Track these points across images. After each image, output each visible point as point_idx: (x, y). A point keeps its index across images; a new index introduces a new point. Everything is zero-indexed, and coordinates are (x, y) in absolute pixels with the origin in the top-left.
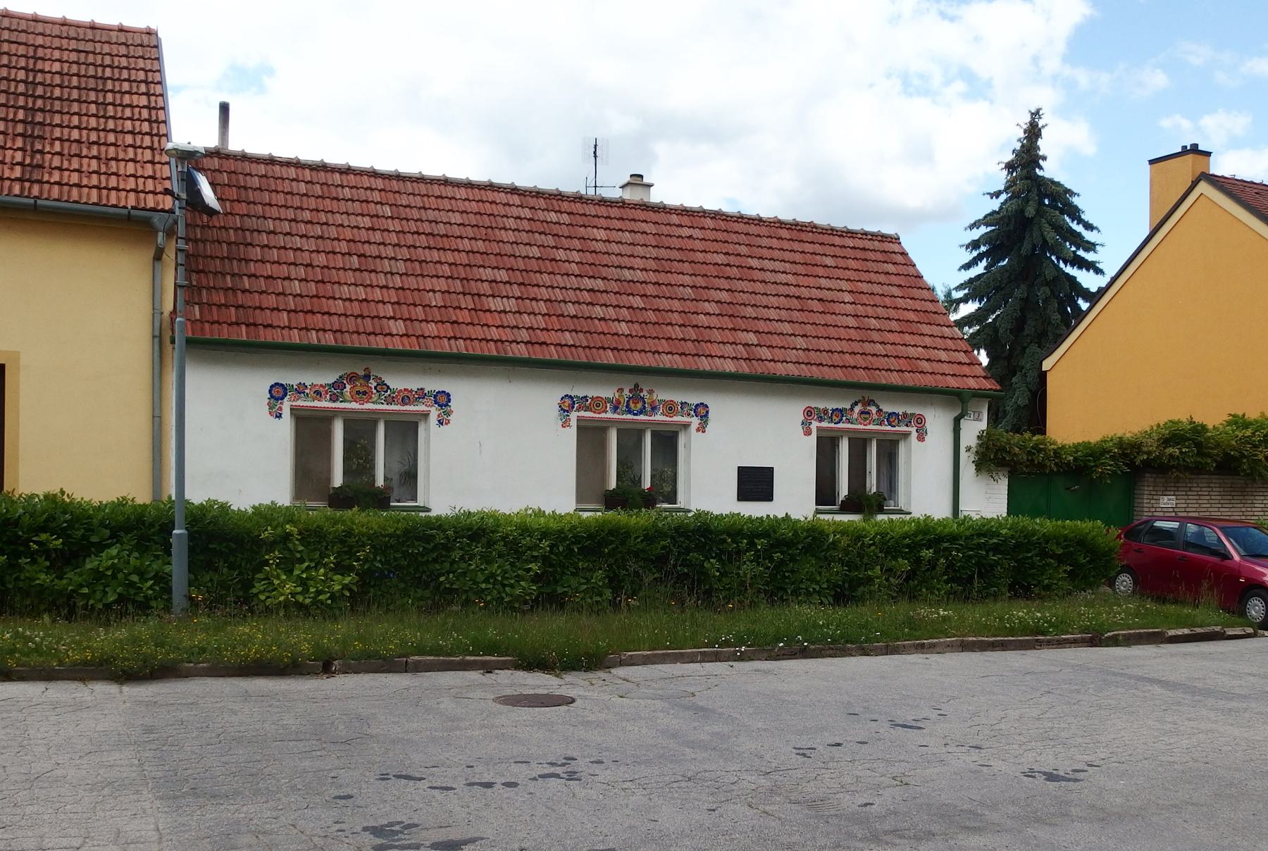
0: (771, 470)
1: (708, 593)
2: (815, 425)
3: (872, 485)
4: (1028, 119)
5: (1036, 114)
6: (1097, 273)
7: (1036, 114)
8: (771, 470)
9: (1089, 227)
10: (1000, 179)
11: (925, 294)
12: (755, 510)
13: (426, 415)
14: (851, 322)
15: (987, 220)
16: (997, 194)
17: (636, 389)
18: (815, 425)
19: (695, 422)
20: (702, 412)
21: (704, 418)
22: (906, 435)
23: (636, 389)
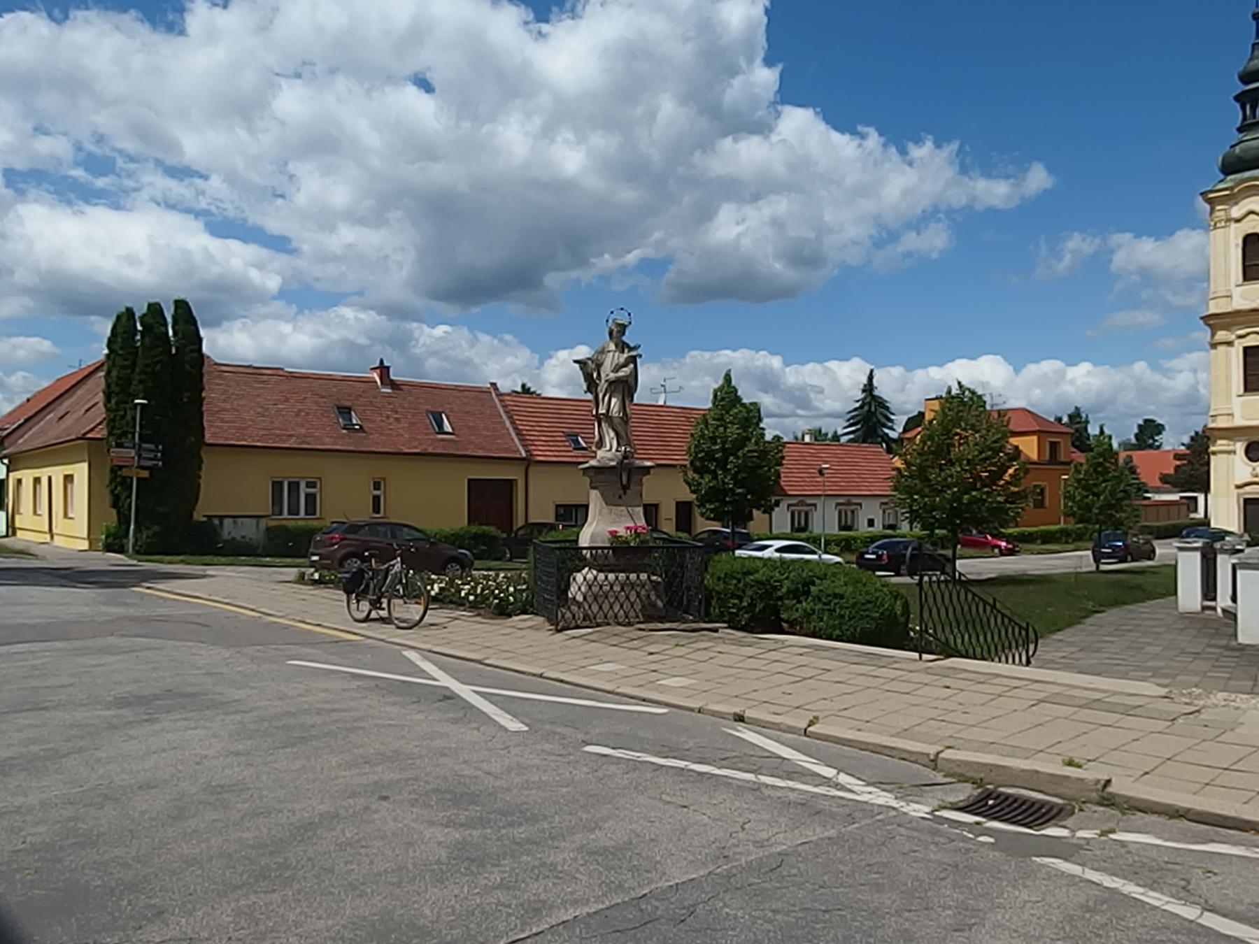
3: (849, 523)
10: (860, 396)
16: (858, 401)
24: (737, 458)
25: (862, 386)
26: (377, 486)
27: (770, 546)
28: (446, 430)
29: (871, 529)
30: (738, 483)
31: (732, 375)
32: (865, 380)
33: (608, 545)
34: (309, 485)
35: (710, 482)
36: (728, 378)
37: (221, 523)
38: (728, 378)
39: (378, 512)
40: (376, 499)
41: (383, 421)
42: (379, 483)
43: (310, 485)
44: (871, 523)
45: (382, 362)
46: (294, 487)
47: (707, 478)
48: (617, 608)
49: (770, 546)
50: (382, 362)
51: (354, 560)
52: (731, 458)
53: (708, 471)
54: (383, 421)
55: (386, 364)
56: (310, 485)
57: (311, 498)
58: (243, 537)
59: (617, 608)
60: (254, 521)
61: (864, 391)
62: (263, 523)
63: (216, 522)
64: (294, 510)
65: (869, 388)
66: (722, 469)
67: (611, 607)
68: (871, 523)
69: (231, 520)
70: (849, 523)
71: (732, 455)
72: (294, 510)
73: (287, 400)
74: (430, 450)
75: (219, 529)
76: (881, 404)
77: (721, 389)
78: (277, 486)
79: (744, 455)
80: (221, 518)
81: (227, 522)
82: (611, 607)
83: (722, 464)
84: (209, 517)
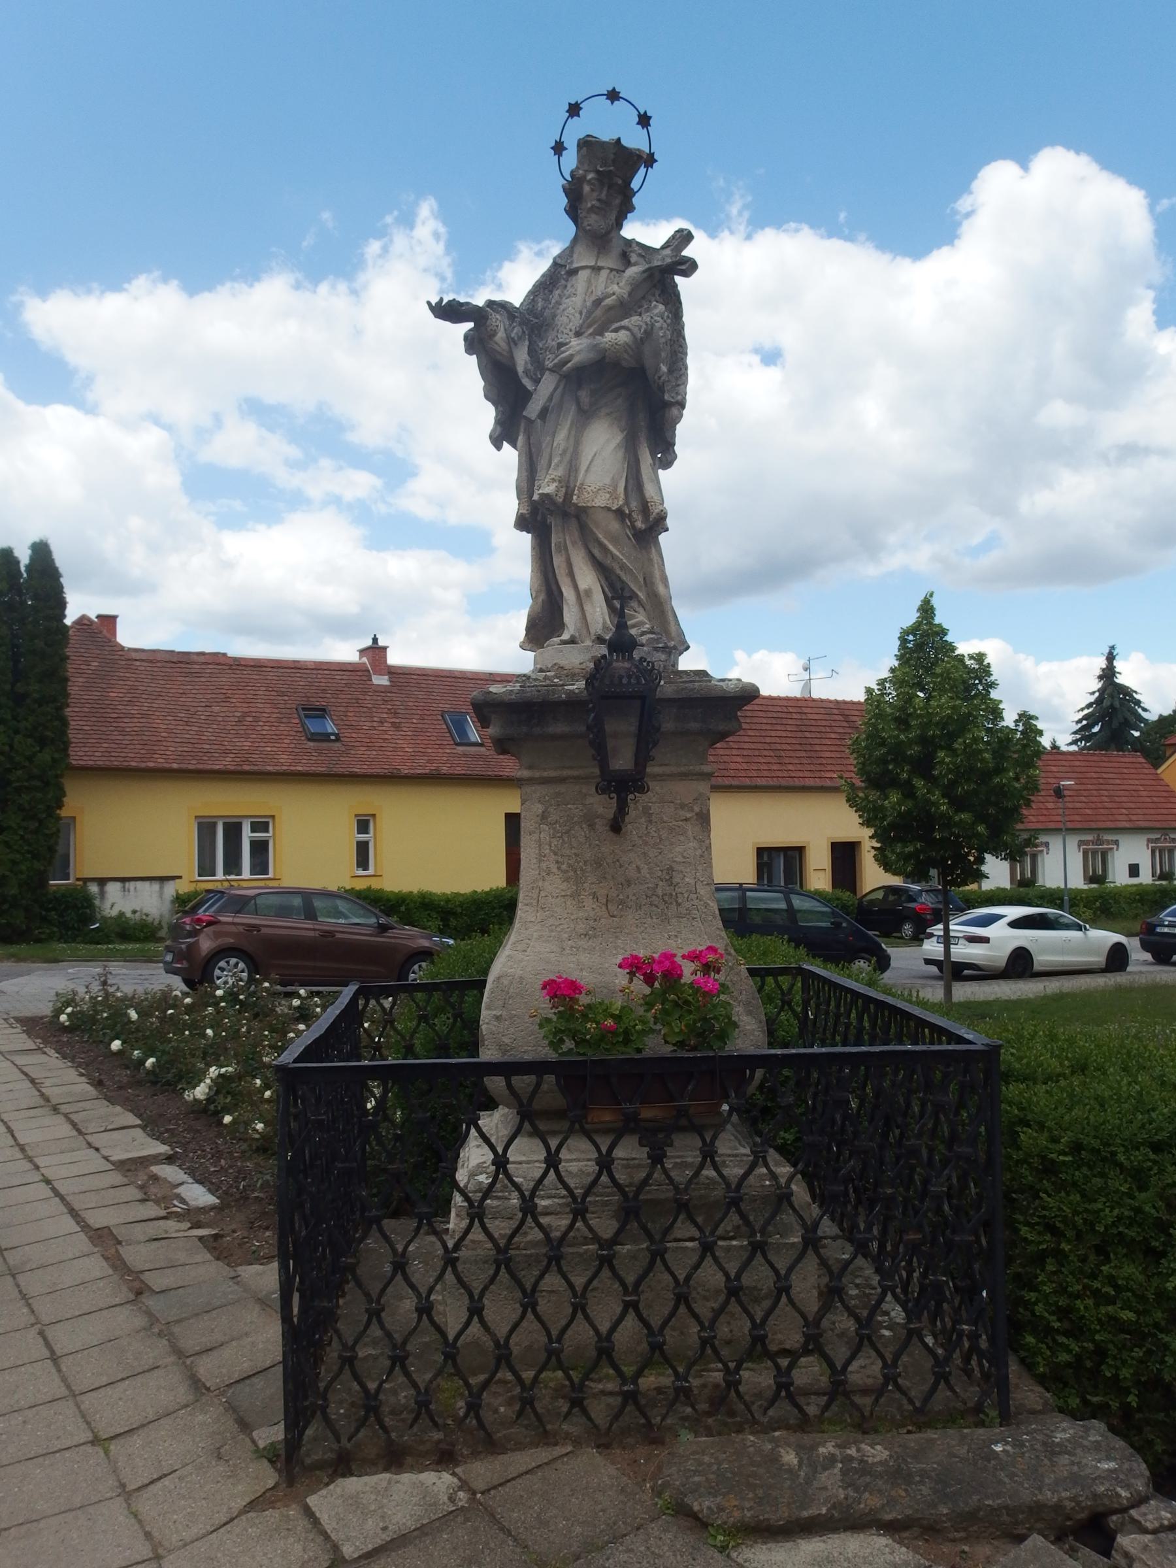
0: (1138, 865)
1: (251, 1228)
2: (1150, 845)
3: (1167, 868)
4: (1107, 650)
5: (1113, 648)
6: (932, 609)
7: (1113, 648)
8: (1138, 865)
9: (1145, 710)
10: (1096, 685)
11: (1166, 788)
12: (1135, 881)
13: (1042, 851)
14: (1148, 800)
15: (1089, 706)
16: (1093, 693)
17: (1099, 836)
18: (1150, 845)
19: (1115, 847)
20: (1117, 843)
21: (1118, 845)
22: (1111, 849)
23: (1099, 836)
24: (954, 752)
25: (1098, 672)
26: (363, 825)
27: (1000, 917)
28: (473, 739)
29: (1135, 881)
30: (959, 804)
31: (935, 602)
32: (1102, 663)
33: (546, 1053)
34: (255, 827)
35: (899, 803)
36: (927, 609)
37: (102, 893)
38: (927, 609)
39: (366, 868)
40: (363, 851)
41: (374, 728)
42: (367, 822)
43: (256, 827)
44: (1134, 870)
45: (375, 640)
46: (233, 831)
47: (894, 797)
48: (605, 1309)
49: (1000, 917)
50: (375, 640)
51: (233, 961)
52: (941, 754)
53: (894, 783)
54: (374, 728)
55: (381, 643)
56: (260, 826)
57: (260, 848)
58: (134, 912)
59: (605, 1309)
60: (156, 886)
61: (1100, 678)
62: (170, 889)
63: (94, 888)
64: (232, 864)
65: (1108, 674)
66: (924, 777)
67: (579, 1308)
68: (1134, 870)
69: (118, 885)
70: (1167, 868)
71: (942, 748)
72: (232, 864)
73: (227, 699)
74: (445, 769)
75: (97, 902)
76: (1126, 692)
77: (913, 630)
78: (206, 829)
79: (966, 746)
80: (102, 882)
81: (113, 889)
82: (579, 1308)
83: (924, 766)
84: (86, 880)
